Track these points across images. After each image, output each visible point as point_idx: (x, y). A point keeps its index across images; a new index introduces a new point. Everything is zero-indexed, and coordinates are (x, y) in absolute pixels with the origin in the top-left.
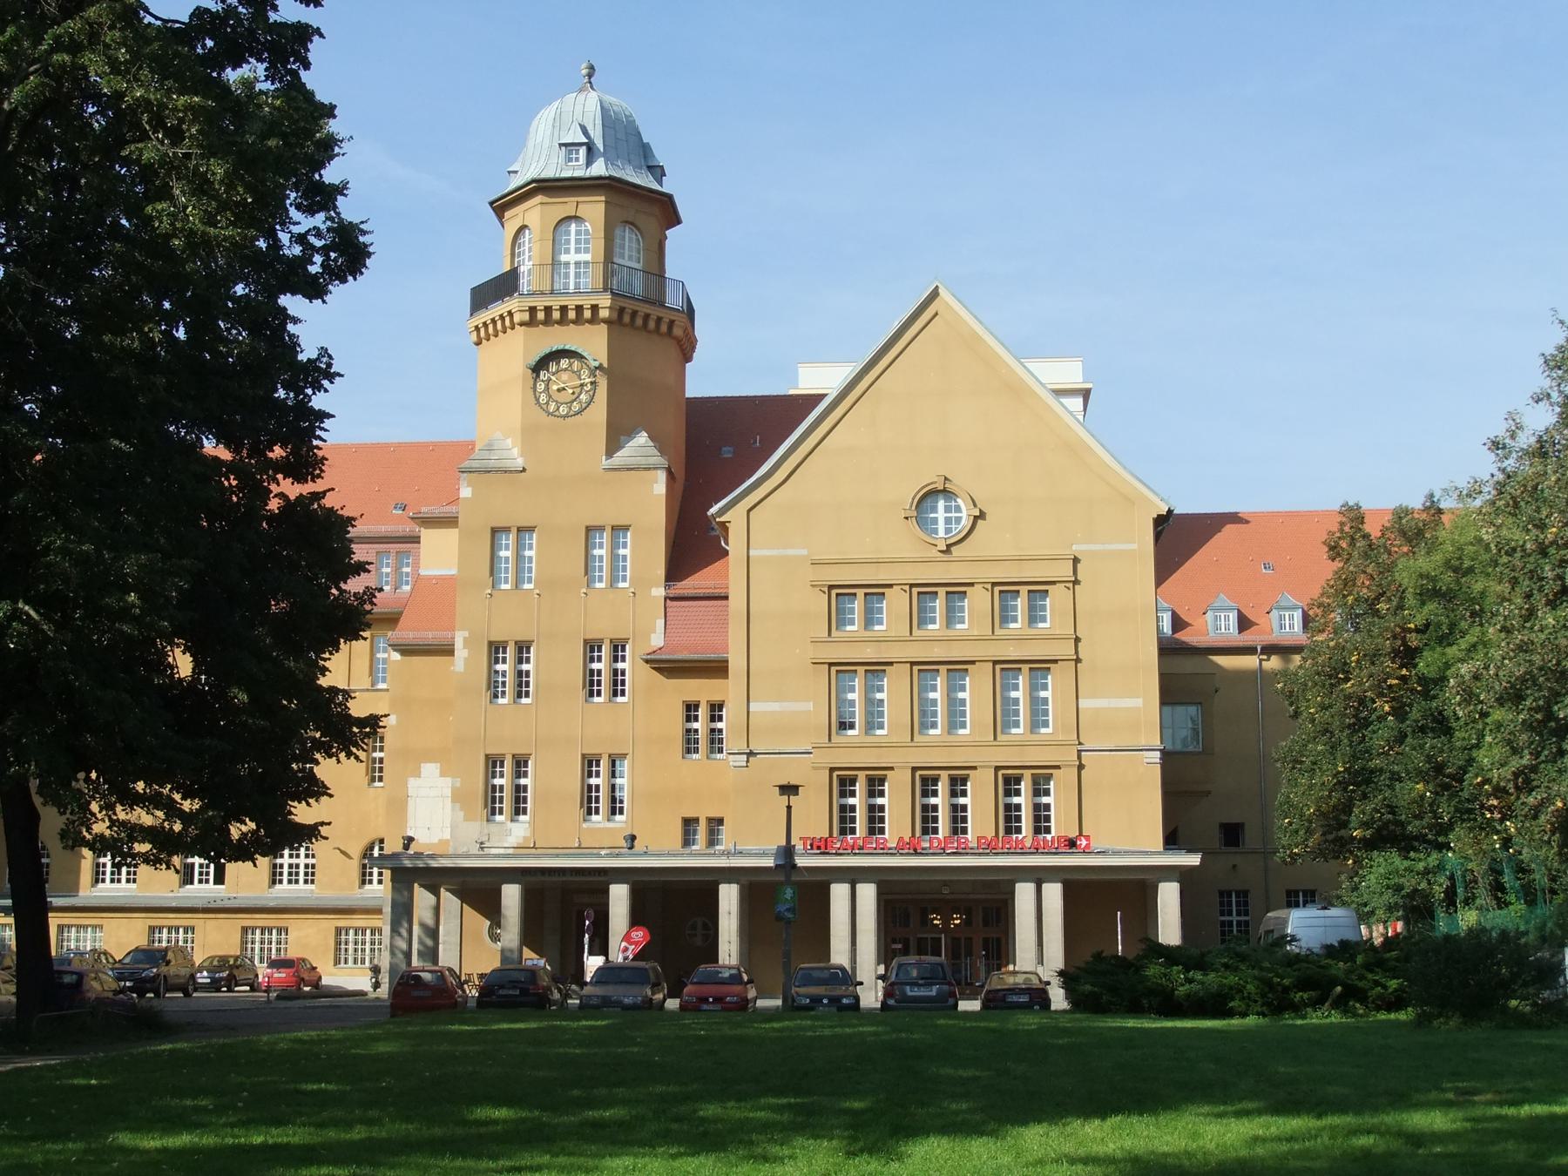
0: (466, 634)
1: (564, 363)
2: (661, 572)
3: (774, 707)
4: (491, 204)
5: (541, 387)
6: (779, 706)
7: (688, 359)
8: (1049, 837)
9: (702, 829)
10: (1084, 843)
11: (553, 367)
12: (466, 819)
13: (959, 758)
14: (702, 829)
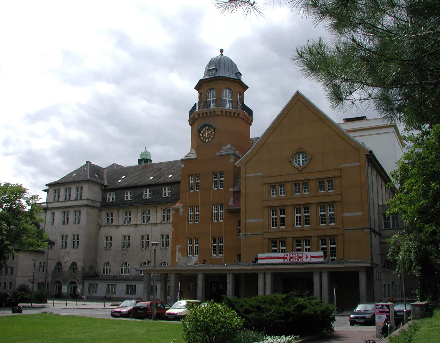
3: (253, 220)
7: (251, 125)
12: (182, 256)
13: (305, 234)
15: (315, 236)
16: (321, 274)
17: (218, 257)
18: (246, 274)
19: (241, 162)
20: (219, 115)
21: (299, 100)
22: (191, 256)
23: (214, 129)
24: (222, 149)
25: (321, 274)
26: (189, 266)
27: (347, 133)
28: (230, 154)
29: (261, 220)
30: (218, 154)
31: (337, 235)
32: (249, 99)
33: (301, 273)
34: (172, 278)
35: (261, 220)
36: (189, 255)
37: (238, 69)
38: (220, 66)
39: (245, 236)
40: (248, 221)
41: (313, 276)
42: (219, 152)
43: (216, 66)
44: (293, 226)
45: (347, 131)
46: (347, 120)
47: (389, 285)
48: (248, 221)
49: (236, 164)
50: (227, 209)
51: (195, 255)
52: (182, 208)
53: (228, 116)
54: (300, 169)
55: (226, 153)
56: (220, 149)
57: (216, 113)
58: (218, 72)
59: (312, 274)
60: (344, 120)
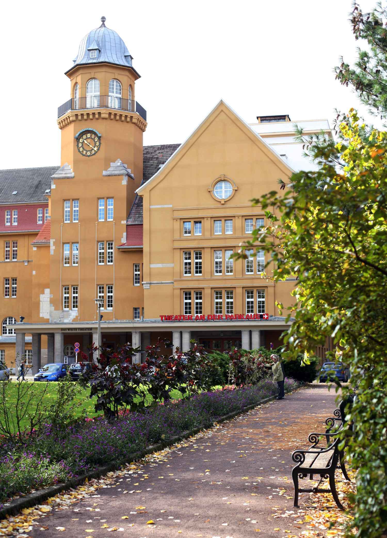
0: (54, 240)
1: (89, 135)
2: (124, 214)
3: (160, 266)
4: (66, 74)
5: (80, 145)
6: (162, 265)
7: (144, 131)
8: (253, 314)
9: (44, 338)
10: (266, 316)
11: (84, 137)
12: (55, 309)
13: (228, 284)
14: (44, 338)
15: (240, 287)
16: (250, 332)
17: (106, 311)
18: (151, 333)
19: (144, 189)
20: (106, 119)
21: (222, 111)
22: (67, 309)
23: (99, 138)
24: (110, 166)
25: (250, 332)
26: (65, 324)
27: (280, 157)
28: (122, 175)
29: (171, 265)
30: (104, 173)
31: (267, 287)
32: (142, 93)
33: (222, 332)
34: (58, 339)
35: (171, 265)
36: (64, 309)
37: (128, 52)
38: (105, 46)
39: (149, 285)
40: (152, 266)
41: (241, 336)
42: (106, 170)
43: (98, 45)
44: (212, 274)
45: (262, 136)
46: (263, 119)
47: (319, 348)
48: (152, 266)
49: (137, 191)
50: (119, 249)
51: (73, 309)
52: (54, 245)
53: (117, 120)
54: (223, 202)
55: (117, 172)
56: (107, 166)
57: (103, 116)
58: (102, 55)
59: (239, 333)
60: (258, 118)
